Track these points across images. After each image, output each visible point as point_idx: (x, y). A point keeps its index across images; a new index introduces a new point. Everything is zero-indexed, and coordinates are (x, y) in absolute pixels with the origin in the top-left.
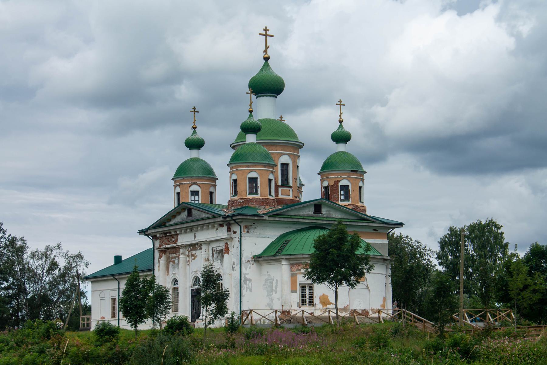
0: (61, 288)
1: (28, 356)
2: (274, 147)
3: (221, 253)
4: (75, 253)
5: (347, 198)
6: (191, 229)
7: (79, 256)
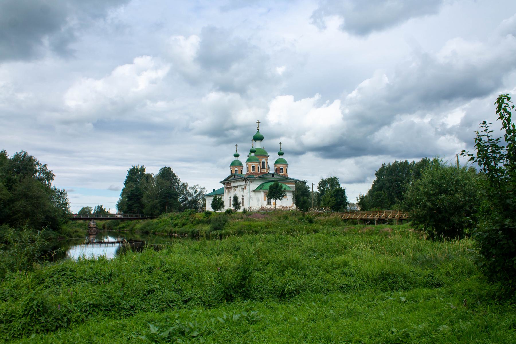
0: (198, 198)
1: (184, 221)
3: (244, 189)
4: (203, 187)
5: (282, 172)
6: (235, 182)
7: (204, 188)
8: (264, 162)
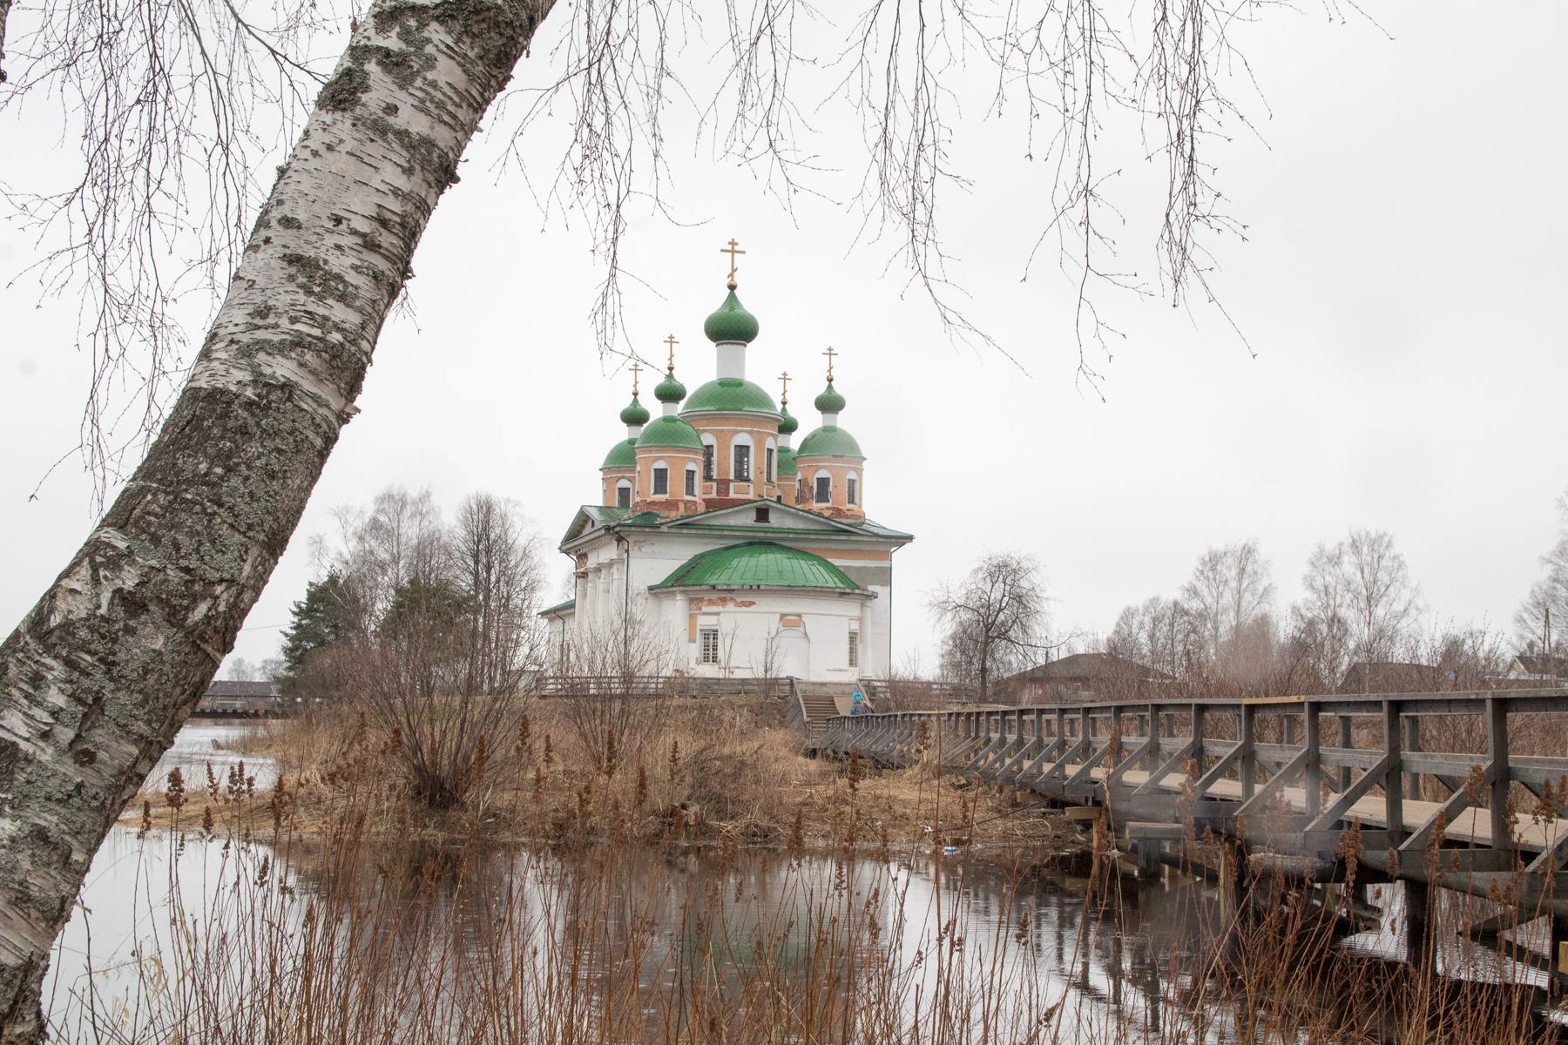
2: (724, 422)
8: (693, 472)
